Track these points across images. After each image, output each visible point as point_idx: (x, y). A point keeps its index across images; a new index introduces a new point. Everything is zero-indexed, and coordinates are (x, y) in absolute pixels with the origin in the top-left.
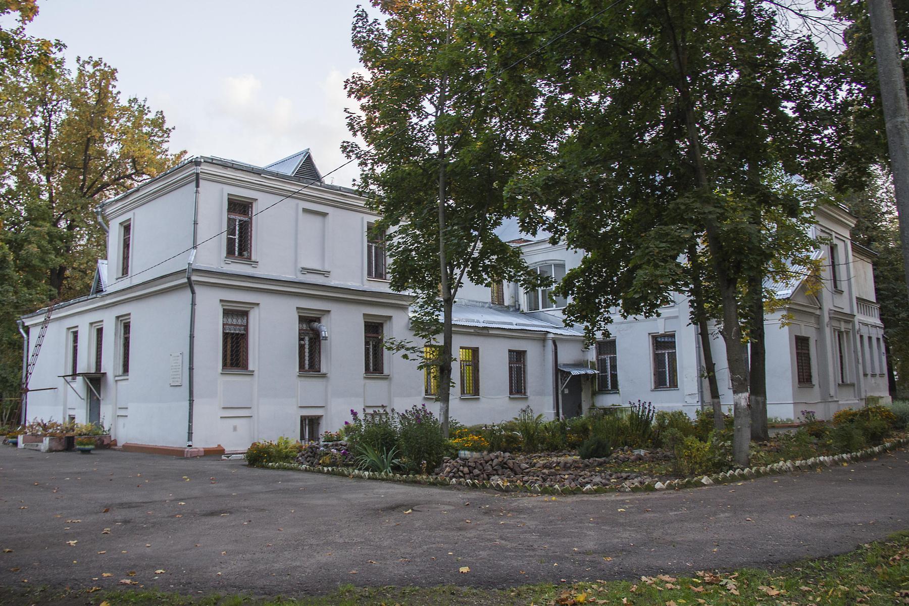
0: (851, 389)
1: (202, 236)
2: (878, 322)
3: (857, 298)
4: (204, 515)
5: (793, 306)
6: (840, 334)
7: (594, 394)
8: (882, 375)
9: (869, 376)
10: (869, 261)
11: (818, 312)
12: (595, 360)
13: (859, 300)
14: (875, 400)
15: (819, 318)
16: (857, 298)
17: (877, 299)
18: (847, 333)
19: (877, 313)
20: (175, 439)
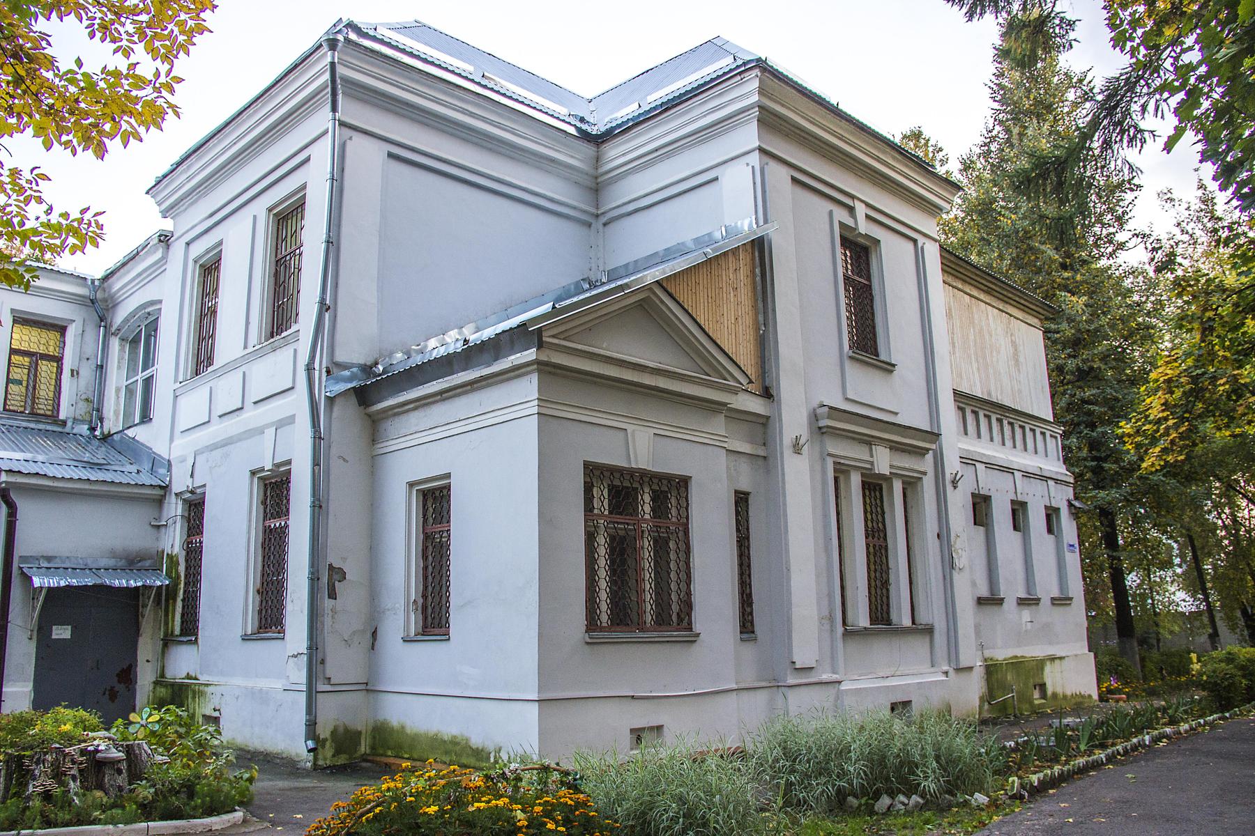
0: (919, 646)
1: (762, 454)
2: (1056, 467)
3: (958, 395)
4: (1061, 658)
5: (558, 359)
6: (874, 488)
7: (168, 642)
8: (1062, 601)
9: (1010, 604)
10: (1035, 321)
11: (754, 405)
12: (177, 550)
13: (963, 399)
14: (1031, 670)
15: (762, 427)
16: (958, 395)
17: (1055, 415)
18: (911, 484)
19: (1054, 447)
20: (305, 658)
